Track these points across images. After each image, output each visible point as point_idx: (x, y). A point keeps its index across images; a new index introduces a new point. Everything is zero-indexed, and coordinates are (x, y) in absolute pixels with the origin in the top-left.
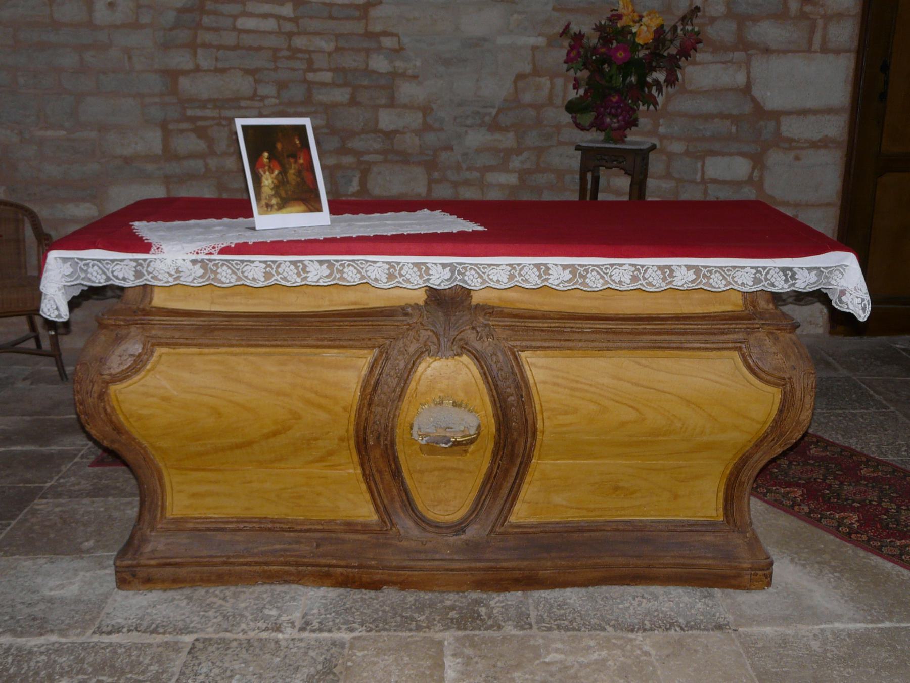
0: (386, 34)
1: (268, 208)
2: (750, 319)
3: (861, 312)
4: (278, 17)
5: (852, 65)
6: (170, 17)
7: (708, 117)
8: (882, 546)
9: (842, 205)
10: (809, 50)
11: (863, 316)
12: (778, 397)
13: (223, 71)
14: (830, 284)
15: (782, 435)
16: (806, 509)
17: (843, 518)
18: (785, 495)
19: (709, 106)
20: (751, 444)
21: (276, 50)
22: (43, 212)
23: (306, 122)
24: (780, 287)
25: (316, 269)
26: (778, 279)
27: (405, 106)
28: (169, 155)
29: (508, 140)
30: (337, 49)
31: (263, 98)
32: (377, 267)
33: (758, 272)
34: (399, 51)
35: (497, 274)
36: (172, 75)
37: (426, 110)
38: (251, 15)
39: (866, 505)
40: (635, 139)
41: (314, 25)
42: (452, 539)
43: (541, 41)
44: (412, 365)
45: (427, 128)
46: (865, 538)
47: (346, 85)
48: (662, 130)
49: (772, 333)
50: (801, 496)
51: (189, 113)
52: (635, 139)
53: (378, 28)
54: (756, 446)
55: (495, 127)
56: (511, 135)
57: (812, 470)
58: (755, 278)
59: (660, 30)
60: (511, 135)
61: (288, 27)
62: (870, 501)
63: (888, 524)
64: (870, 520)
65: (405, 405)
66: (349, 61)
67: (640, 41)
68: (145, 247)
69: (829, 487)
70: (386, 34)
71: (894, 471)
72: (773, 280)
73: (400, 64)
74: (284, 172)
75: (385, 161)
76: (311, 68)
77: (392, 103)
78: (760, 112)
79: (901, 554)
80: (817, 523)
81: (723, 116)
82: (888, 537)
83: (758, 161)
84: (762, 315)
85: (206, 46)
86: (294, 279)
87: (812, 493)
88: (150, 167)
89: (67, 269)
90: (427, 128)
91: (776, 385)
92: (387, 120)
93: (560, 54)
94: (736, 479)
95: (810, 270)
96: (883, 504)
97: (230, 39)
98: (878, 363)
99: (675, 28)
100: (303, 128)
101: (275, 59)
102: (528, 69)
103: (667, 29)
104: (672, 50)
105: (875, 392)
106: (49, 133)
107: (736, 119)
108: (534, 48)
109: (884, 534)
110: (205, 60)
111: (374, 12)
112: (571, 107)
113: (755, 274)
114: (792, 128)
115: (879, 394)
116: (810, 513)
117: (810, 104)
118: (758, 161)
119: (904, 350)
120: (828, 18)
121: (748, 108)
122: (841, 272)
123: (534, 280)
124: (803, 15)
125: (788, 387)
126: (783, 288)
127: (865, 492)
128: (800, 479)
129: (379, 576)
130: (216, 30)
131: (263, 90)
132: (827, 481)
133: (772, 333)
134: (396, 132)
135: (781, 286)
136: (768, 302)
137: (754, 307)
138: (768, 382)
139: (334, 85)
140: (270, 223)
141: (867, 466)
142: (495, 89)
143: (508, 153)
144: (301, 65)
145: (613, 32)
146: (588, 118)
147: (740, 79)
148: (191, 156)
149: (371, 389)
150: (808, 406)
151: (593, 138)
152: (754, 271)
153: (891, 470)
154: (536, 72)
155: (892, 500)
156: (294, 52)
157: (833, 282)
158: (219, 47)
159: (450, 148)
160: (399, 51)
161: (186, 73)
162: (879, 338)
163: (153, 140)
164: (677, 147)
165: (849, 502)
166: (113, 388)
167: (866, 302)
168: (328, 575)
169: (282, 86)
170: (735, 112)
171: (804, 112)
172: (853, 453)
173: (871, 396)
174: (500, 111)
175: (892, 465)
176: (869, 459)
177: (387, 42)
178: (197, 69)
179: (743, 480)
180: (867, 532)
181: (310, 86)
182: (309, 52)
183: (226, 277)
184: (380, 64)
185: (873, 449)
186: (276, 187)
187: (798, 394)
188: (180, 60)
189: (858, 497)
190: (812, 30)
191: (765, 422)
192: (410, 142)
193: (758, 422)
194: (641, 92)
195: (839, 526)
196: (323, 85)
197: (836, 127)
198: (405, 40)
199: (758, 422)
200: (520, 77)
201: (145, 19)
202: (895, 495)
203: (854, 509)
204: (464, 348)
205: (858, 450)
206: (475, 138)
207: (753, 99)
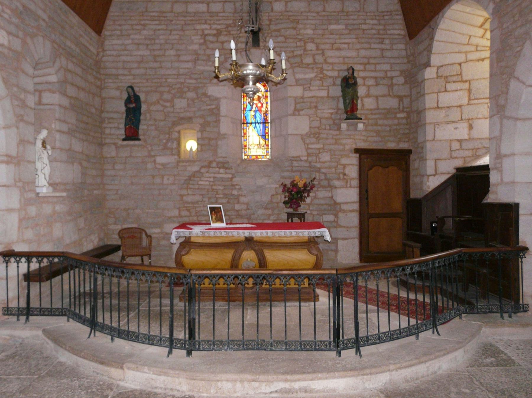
0: (237, 185)
1: (214, 222)
4: (209, 181)
5: (358, 190)
6: (183, 182)
7: (322, 205)
10: (347, 187)
11: (329, 241)
13: (195, 195)
19: (323, 202)
21: (208, 189)
22: (147, 231)
23: (221, 206)
25: (223, 233)
27: (242, 203)
28: (180, 216)
29: (270, 212)
30: (224, 189)
31: (205, 201)
32: (235, 232)
34: (240, 189)
35: (258, 234)
36: (182, 196)
37: (247, 204)
38: (202, 181)
40: (301, 210)
41: (218, 183)
42: (250, 291)
43: (278, 186)
44: (242, 253)
45: (248, 209)
47: (226, 198)
48: (311, 208)
51: (186, 205)
52: (301, 210)
53: (235, 183)
55: (266, 208)
56: (270, 210)
59: (305, 184)
60: (270, 210)
61: (212, 183)
65: (240, 260)
66: (227, 192)
67: (300, 186)
68: (191, 229)
70: (237, 185)
73: (240, 193)
74: (217, 215)
75: (237, 218)
76: (217, 194)
77: (238, 202)
78: (335, 203)
81: (326, 204)
83: (336, 216)
85: (190, 188)
86: (219, 235)
88: (175, 219)
89: (176, 233)
90: (248, 209)
92: (237, 207)
93: (281, 189)
97: (197, 187)
99: (309, 183)
100: (220, 208)
101: (208, 191)
102: (274, 193)
103: (307, 183)
104: (308, 188)
106: (150, 211)
107: (330, 205)
108: (276, 188)
110: (190, 192)
111: (234, 180)
112: (285, 203)
114: (344, 207)
117: (349, 201)
118: (336, 216)
120: (351, 179)
121: (332, 202)
123: (265, 235)
124: (344, 179)
129: (235, 299)
130: (193, 184)
131: (204, 199)
134: (239, 210)
135: (313, 235)
139: (223, 198)
140: (214, 225)
142: (266, 199)
143: (270, 215)
144: (215, 193)
145: (294, 185)
146: (288, 205)
147: (330, 195)
148: (186, 217)
149: (233, 259)
151: (290, 210)
154: (277, 194)
156: (213, 190)
158: (194, 189)
159: (254, 214)
160: (240, 189)
161: (185, 195)
163: (176, 213)
164: (315, 213)
166: (183, 257)
168: (224, 299)
169: (210, 198)
170: (329, 203)
171: (346, 203)
174: (267, 204)
177: (237, 187)
178: (188, 194)
181: (217, 198)
182: (217, 189)
183: (206, 234)
184: (235, 192)
186: (215, 218)
188: (184, 192)
190: (347, 182)
192: (243, 213)
194: (302, 199)
196: (220, 198)
197: (356, 206)
198: (242, 187)
200: (273, 195)
201: (176, 182)
204: (252, 249)
206: (260, 212)
207: (334, 200)
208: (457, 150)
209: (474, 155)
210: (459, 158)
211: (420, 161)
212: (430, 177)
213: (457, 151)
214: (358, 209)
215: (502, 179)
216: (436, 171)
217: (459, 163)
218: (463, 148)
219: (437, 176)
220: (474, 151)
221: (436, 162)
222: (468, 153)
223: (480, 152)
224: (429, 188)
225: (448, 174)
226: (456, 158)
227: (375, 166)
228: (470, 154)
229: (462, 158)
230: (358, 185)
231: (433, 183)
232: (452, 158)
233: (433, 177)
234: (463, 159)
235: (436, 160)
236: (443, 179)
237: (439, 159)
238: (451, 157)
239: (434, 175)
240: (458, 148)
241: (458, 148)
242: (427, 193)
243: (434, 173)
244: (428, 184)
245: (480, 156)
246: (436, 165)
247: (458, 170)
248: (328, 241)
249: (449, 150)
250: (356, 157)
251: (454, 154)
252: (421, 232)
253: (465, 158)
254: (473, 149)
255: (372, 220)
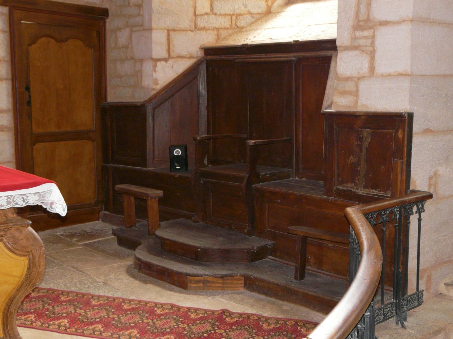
2: (5, 224)
3: (63, 212)
8: (83, 331)
9: (16, 162)
11: (63, 213)
12: (27, 262)
14: (44, 199)
15: (31, 282)
16: (40, 324)
17: (60, 323)
18: (25, 320)
20: (15, 290)
24: (21, 204)
26: (19, 200)
33: (9, 198)
39: (69, 314)
46: (74, 329)
49: (18, 229)
50: (35, 318)
54: (18, 290)
57: (36, 304)
58: (7, 201)
62: (71, 312)
63: (83, 320)
64: (73, 321)
69: (48, 310)
71: (77, 295)
72: (17, 201)
79: (94, 332)
80: (47, 329)
82: (85, 326)
84: (11, 221)
87: (40, 315)
91: (25, 256)
94: (8, 312)
95: (35, 194)
96: (77, 311)
98: (51, 244)
105: (54, 259)
109: (83, 325)
113: (7, 199)
115: (57, 259)
116: (42, 325)
119: (62, 235)
122: (50, 194)
125: (31, 256)
126: (22, 205)
127: (67, 308)
128: (31, 310)
132: (46, 307)
133: (18, 229)
135: (21, 204)
136: (13, 214)
137: (6, 217)
138: (20, 255)
141: (63, 295)
150: (42, 264)
152: (6, 198)
153: (76, 295)
155: (81, 309)
157: (46, 199)
162: (47, 231)
165: (60, 314)
167: (64, 207)
172: (54, 291)
173: (53, 261)
175: (75, 292)
176: (63, 292)
179: (12, 311)
180: (74, 327)
185: (63, 287)
187: (37, 258)
189: (64, 311)
191: (21, 276)
193: (17, 277)
195: (59, 327)
199: (17, 277)
202: (81, 306)
203: (64, 318)
205: (56, 289)
208: (206, 14)
209: (234, 26)
210: (209, 29)
211: (132, 31)
212: (159, 63)
213: (206, 16)
214: (12, 125)
215: (372, 69)
216: (169, 50)
217: (210, 40)
218: (214, 12)
219: (170, 62)
220: (234, 17)
221: (168, 35)
222: (224, 22)
223: (242, 22)
224: (157, 84)
225: (191, 57)
226: (204, 29)
227: (42, 37)
228: (227, 25)
229: (213, 29)
230: (10, 76)
231: (164, 74)
232: (196, 28)
233: (163, 63)
234: (216, 32)
235: (168, 31)
236: (181, 67)
237: (174, 30)
238: (195, 27)
239: (166, 60)
240: (208, 10)
241: (208, 10)
242: (153, 93)
243: (165, 55)
244: (155, 75)
245: (242, 28)
246: (168, 40)
247: (208, 51)
248: (57, 215)
249: (191, 14)
250: (2, 14)
251: (201, 23)
252: (145, 166)
253: (218, 29)
254: (231, 15)
255: (39, 146)
